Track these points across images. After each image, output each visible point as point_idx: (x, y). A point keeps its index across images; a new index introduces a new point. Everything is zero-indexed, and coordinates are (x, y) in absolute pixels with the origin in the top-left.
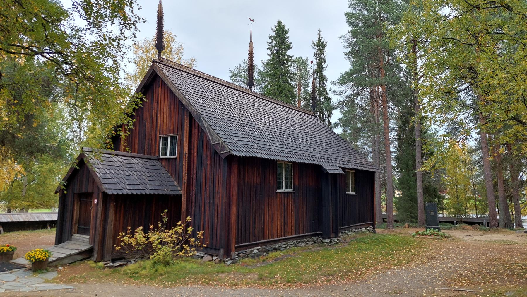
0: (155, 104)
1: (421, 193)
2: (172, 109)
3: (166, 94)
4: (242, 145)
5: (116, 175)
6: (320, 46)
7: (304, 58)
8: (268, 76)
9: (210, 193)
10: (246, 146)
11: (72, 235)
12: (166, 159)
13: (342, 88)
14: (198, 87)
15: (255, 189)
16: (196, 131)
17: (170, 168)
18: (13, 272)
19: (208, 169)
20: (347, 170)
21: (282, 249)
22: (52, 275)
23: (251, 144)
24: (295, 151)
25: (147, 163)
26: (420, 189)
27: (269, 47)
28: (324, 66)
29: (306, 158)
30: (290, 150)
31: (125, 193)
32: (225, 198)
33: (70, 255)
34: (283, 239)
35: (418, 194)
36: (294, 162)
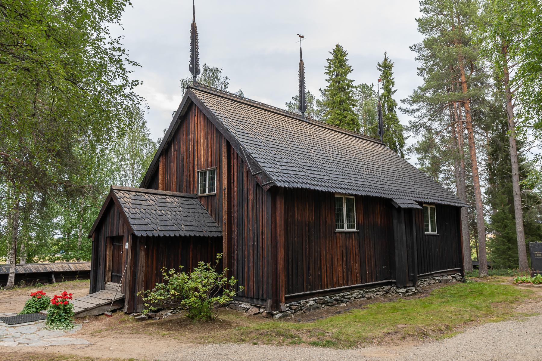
0: (192, 136)
1: (521, 232)
2: (210, 140)
3: (202, 123)
4: (289, 175)
5: (147, 215)
6: (386, 67)
7: (369, 84)
8: (327, 105)
9: (253, 233)
10: (293, 176)
11: (106, 283)
12: (205, 197)
13: (415, 107)
14: (238, 112)
15: (307, 228)
16: (235, 161)
17: (210, 206)
18: (37, 323)
19: (250, 206)
20: (424, 205)
21: (345, 300)
22: (78, 327)
23: (300, 173)
24: (357, 182)
25: (185, 202)
26: (520, 227)
27: (327, 71)
28: (393, 89)
29: (372, 190)
30: (352, 181)
31: (156, 235)
32: (270, 239)
33: (99, 306)
34: (347, 288)
35: (518, 234)
36: (355, 195)
